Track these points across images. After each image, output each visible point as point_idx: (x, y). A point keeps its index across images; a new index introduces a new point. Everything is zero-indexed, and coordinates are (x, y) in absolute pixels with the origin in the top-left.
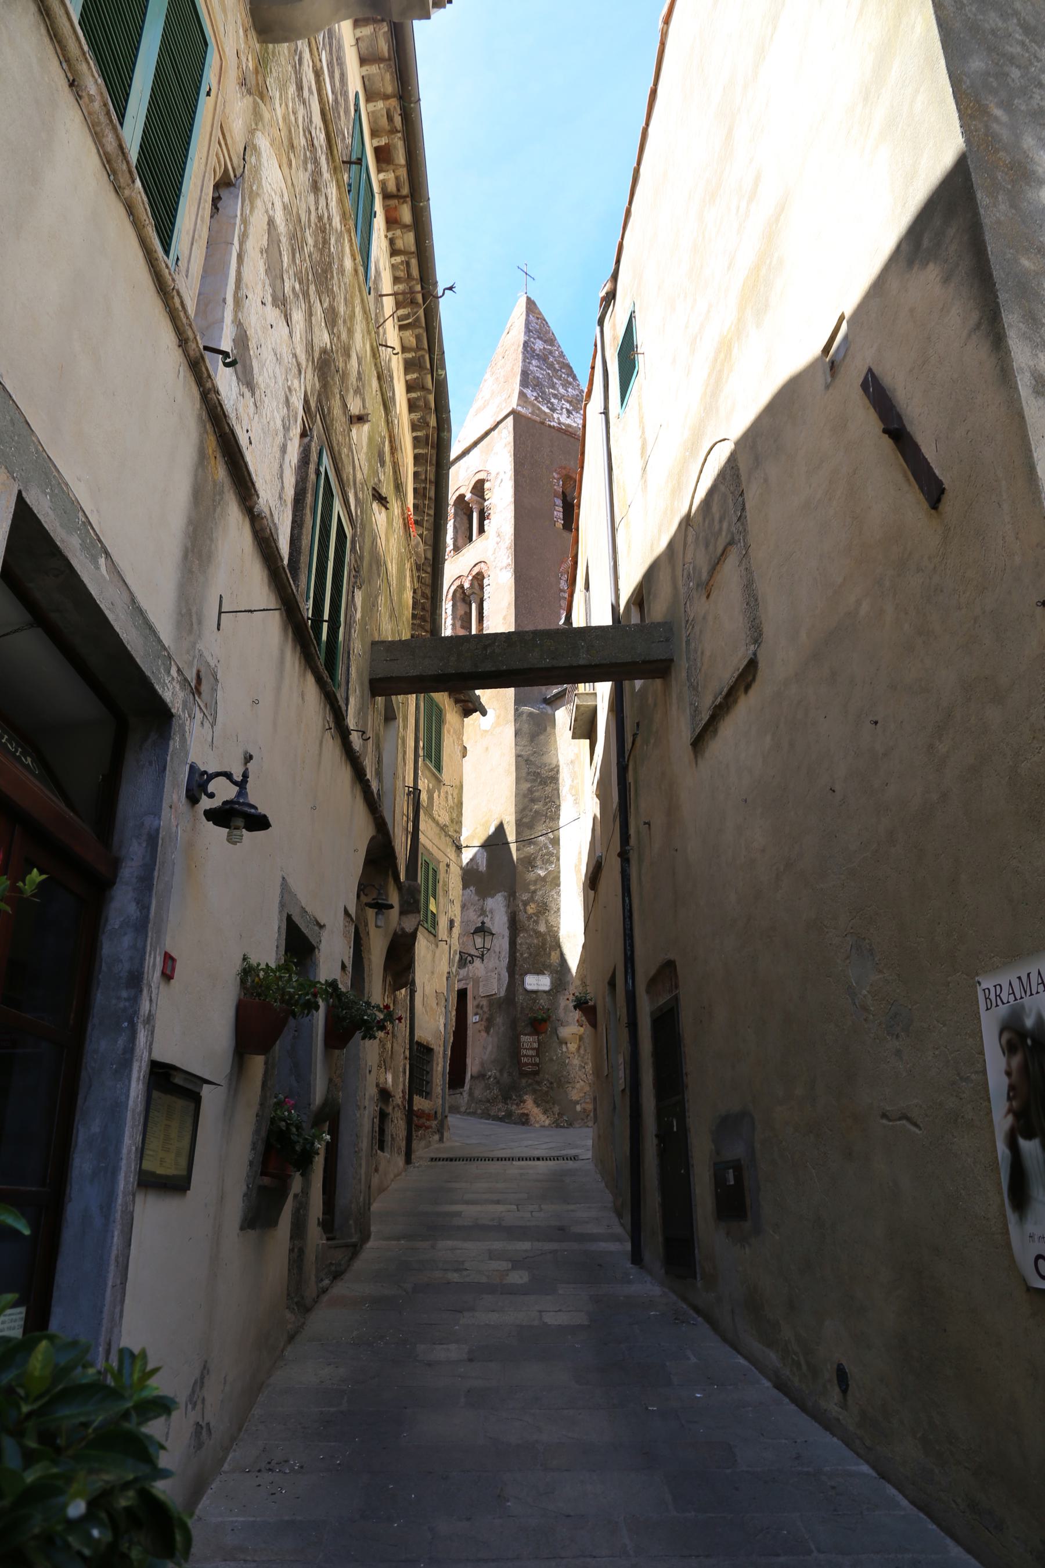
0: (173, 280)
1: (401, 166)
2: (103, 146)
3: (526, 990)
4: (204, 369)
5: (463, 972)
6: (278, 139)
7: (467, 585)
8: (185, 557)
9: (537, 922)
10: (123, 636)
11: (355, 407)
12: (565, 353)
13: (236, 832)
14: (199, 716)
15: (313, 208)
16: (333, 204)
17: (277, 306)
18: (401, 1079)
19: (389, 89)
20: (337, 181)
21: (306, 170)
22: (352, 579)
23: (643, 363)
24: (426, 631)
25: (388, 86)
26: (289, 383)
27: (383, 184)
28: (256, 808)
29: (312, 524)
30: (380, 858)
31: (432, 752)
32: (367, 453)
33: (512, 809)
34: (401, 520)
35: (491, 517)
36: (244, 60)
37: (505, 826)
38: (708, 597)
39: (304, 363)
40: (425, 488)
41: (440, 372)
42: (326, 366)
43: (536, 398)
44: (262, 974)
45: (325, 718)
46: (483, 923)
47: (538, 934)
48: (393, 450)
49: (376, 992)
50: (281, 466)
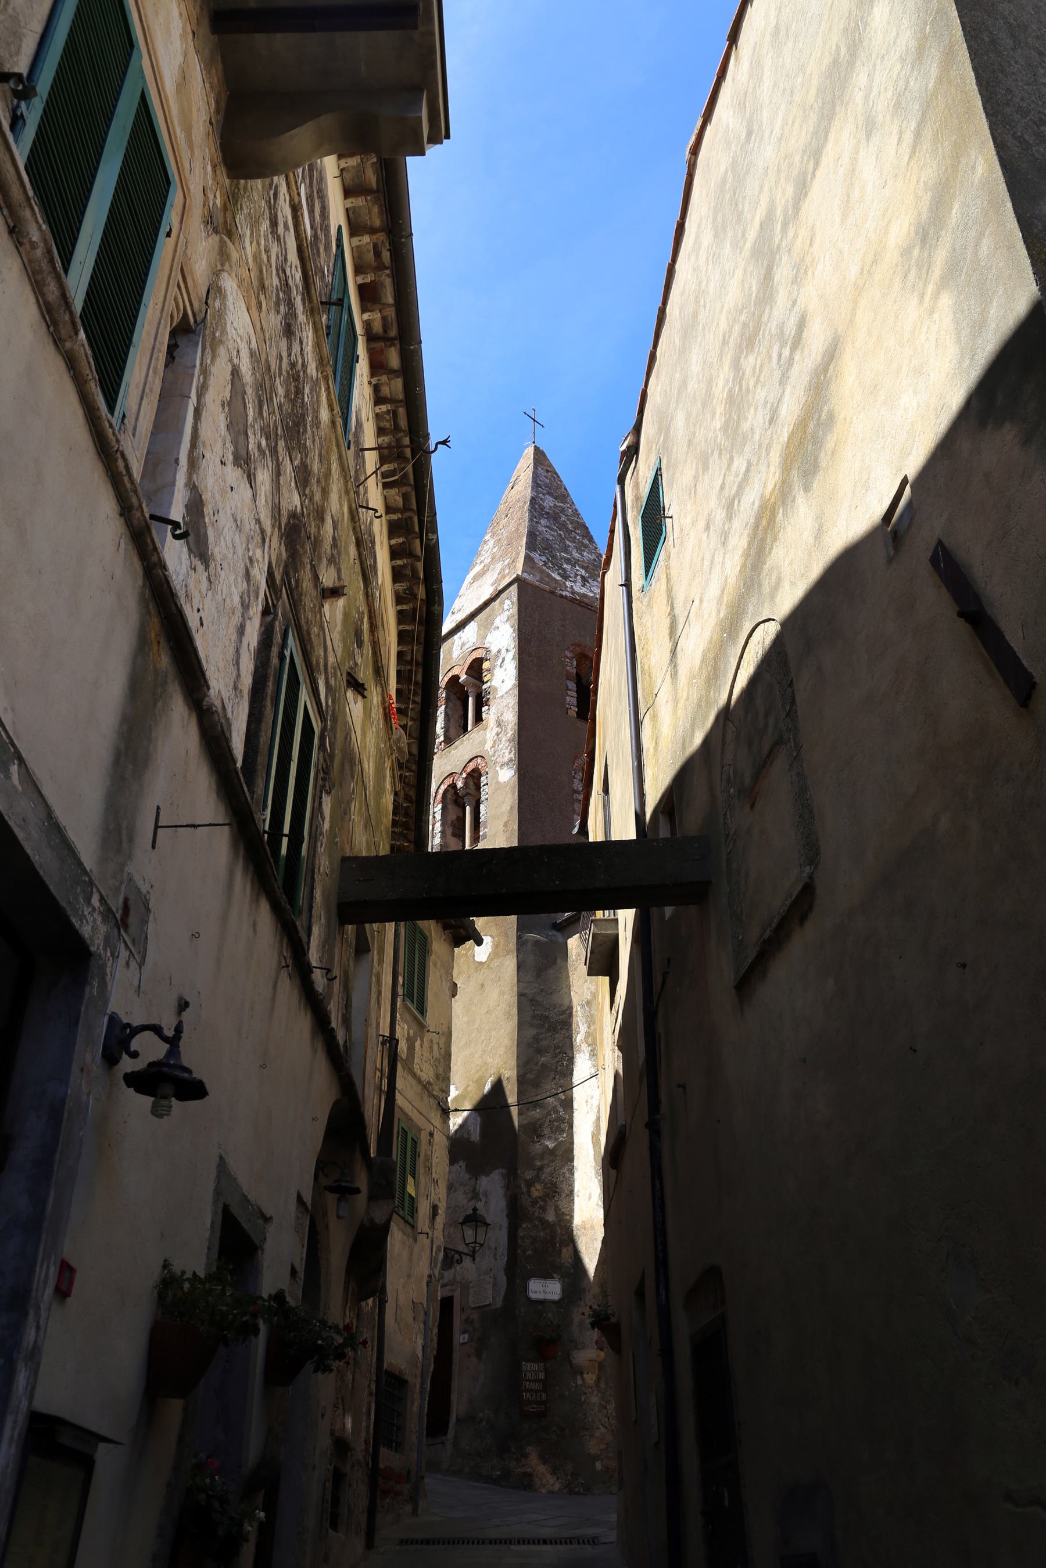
0: (118, 441)
1: (389, 305)
2: (43, 295)
3: (529, 1299)
4: (149, 540)
5: (448, 1275)
6: (247, 279)
7: (460, 784)
8: (117, 762)
9: (543, 1209)
10: (35, 858)
11: (328, 578)
12: (580, 511)
13: (163, 1102)
14: (124, 954)
15: (285, 354)
16: (309, 348)
17: (239, 466)
18: (364, 1424)
19: (377, 223)
20: (314, 324)
21: (278, 312)
22: (320, 782)
23: (672, 528)
24: (409, 841)
25: (375, 218)
26: (251, 554)
27: (368, 325)
28: (189, 1071)
29: (274, 717)
30: (345, 1125)
31: (415, 990)
32: (342, 632)
33: (513, 1062)
34: (381, 710)
35: (491, 703)
36: (211, 197)
37: (505, 1083)
38: (752, 806)
39: (268, 530)
40: (411, 671)
41: (431, 536)
42: (294, 532)
43: (545, 564)
44: (186, 1285)
45: (281, 953)
46: (475, 1209)
47: (545, 1224)
48: (373, 628)
49: (335, 1307)
50: (237, 651)
